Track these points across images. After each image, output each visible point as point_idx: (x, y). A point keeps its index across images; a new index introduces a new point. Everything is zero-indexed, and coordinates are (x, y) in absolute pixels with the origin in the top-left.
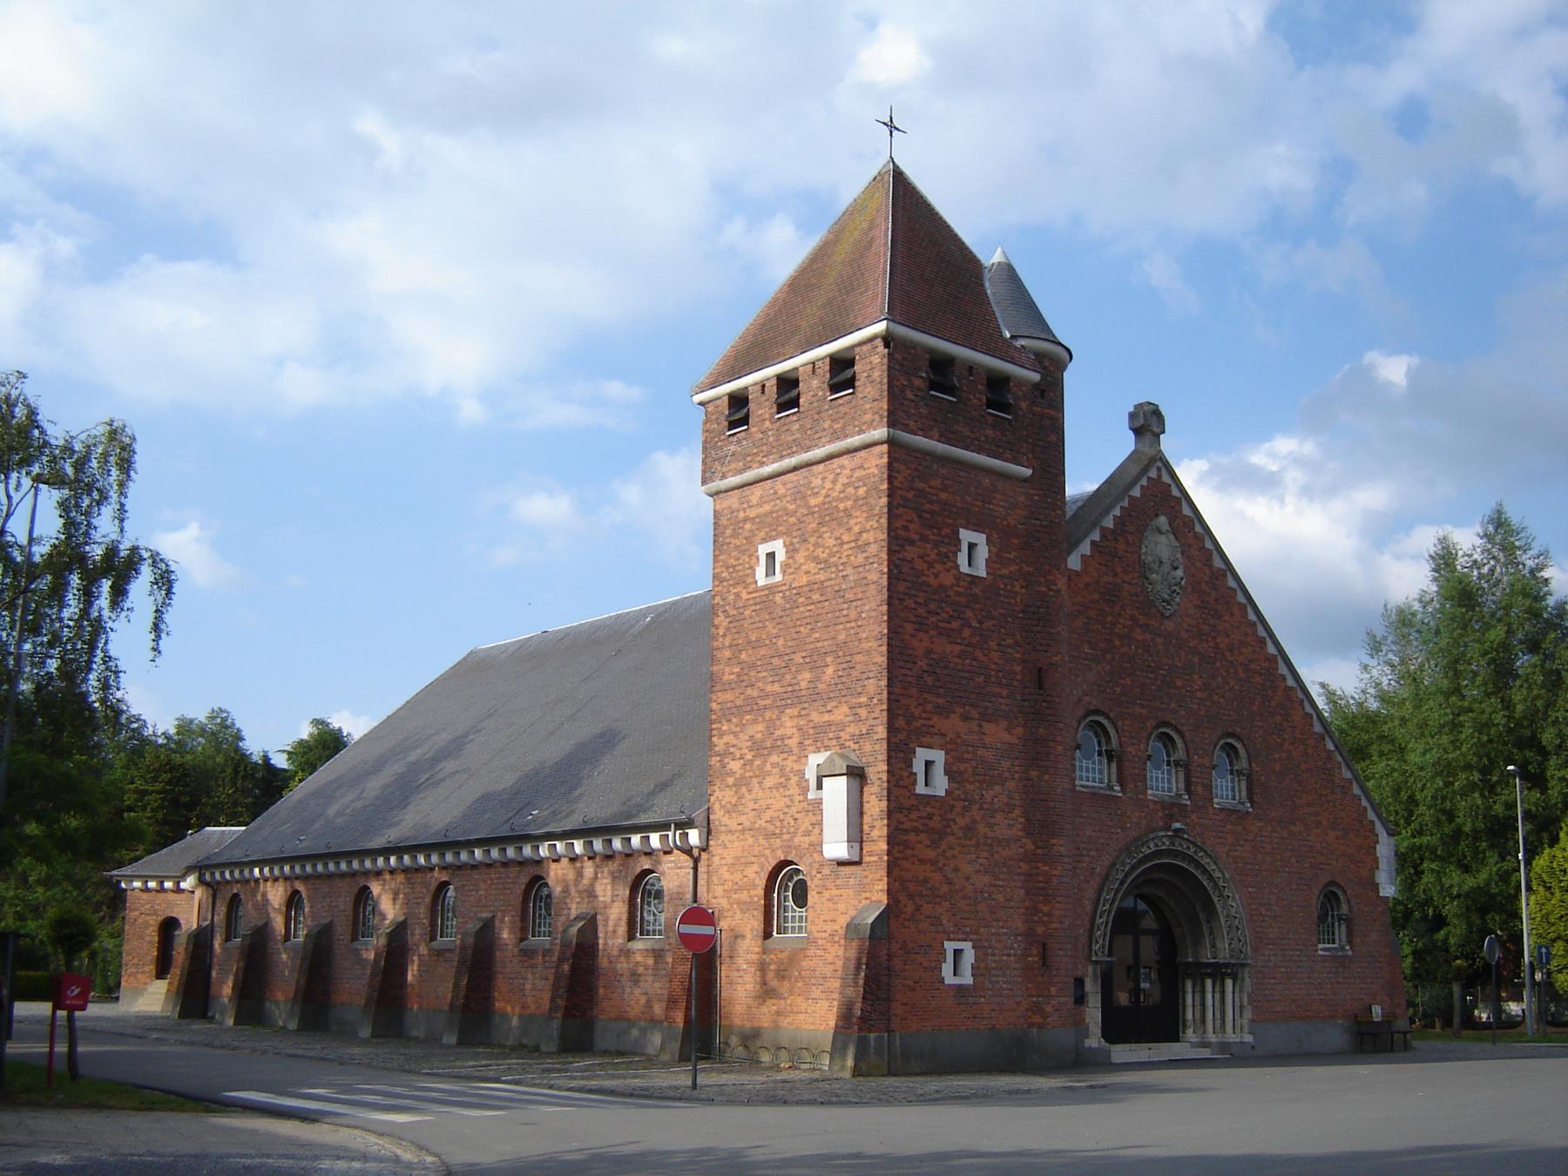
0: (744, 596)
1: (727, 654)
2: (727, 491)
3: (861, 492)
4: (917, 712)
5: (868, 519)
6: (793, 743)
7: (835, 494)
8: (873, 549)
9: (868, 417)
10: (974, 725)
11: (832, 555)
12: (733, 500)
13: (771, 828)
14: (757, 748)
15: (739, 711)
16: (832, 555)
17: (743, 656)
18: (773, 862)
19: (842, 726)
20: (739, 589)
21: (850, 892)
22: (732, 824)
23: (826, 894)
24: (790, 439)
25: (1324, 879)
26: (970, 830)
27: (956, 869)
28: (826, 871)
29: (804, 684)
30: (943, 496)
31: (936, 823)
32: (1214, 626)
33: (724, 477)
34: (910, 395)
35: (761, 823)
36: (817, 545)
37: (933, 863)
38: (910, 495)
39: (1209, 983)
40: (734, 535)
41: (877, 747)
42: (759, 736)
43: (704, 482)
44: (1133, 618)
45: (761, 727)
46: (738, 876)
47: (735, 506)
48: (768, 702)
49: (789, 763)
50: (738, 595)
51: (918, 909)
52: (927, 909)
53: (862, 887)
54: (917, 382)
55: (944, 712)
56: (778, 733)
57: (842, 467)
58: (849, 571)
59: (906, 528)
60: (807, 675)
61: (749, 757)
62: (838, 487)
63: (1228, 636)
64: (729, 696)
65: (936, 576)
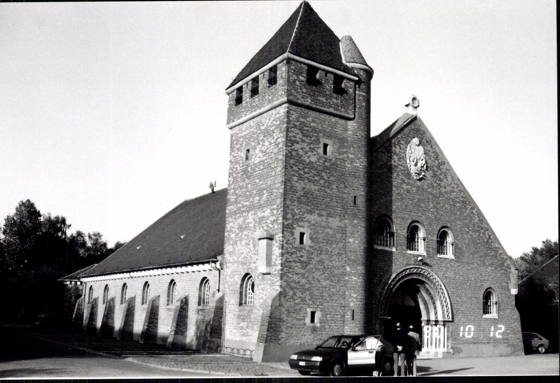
0: (239, 168)
1: (232, 191)
2: (236, 126)
3: (278, 123)
4: (297, 212)
5: (280, 133)
6: (251, 225)
7: (269, 124)
8: (281, 145)
9: (280, 93)
10: (324, 218)
11: (267, 149)
12: (236, 130)
13: (243, 261)
14: (241, 228)
15: (235, 213)
16: (267, 149)
17: (237, 192)
18: (243, 274)
19: (268, 218)
20: (237, 166)
21: (268, 286)
22: (231, 259)
23: (260, 287)
24: (255, 104)
25: (486, 286)
26: (321, 262)
27: (314, 278)
28: (260, 277)
29: (256, 202)
30: (312, 124)
31: (304, 259)
32: (440, 184)
33: (233, 121)
34: (298, 83)
35: (240, 259)
36: (263, 145)
37: (303, 275)
38: (298, 124)
39: (99, 324)
40: (237, 144)
41: (279, 226)
42: (241, 223)
43: (228, 123)
44: (402, 180)
45: (242, 219)
46: (232, 280)
47: (238, 132)
48: (244, 209)
49: (250, 234)
50: (237, 168)
51: (295, 294)
52: (299, 294)
53: (272, 284)
54: (301, 78)
55: (310, 212)
56: (247, 221)
57: (272, 114)
58: (273, 155)
59: (295, 137)
60: (257, 198)
61: (237, 232)
62: (271, 121)
63: (445, 188)
64: (232, 207)
65: (309, 157)
